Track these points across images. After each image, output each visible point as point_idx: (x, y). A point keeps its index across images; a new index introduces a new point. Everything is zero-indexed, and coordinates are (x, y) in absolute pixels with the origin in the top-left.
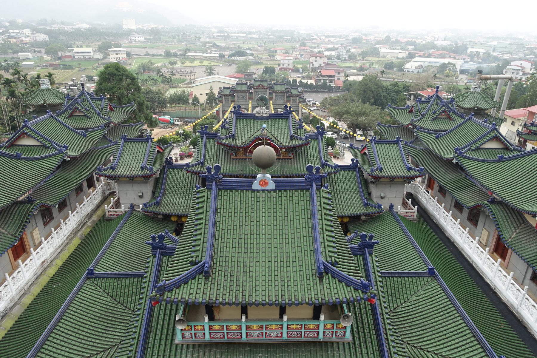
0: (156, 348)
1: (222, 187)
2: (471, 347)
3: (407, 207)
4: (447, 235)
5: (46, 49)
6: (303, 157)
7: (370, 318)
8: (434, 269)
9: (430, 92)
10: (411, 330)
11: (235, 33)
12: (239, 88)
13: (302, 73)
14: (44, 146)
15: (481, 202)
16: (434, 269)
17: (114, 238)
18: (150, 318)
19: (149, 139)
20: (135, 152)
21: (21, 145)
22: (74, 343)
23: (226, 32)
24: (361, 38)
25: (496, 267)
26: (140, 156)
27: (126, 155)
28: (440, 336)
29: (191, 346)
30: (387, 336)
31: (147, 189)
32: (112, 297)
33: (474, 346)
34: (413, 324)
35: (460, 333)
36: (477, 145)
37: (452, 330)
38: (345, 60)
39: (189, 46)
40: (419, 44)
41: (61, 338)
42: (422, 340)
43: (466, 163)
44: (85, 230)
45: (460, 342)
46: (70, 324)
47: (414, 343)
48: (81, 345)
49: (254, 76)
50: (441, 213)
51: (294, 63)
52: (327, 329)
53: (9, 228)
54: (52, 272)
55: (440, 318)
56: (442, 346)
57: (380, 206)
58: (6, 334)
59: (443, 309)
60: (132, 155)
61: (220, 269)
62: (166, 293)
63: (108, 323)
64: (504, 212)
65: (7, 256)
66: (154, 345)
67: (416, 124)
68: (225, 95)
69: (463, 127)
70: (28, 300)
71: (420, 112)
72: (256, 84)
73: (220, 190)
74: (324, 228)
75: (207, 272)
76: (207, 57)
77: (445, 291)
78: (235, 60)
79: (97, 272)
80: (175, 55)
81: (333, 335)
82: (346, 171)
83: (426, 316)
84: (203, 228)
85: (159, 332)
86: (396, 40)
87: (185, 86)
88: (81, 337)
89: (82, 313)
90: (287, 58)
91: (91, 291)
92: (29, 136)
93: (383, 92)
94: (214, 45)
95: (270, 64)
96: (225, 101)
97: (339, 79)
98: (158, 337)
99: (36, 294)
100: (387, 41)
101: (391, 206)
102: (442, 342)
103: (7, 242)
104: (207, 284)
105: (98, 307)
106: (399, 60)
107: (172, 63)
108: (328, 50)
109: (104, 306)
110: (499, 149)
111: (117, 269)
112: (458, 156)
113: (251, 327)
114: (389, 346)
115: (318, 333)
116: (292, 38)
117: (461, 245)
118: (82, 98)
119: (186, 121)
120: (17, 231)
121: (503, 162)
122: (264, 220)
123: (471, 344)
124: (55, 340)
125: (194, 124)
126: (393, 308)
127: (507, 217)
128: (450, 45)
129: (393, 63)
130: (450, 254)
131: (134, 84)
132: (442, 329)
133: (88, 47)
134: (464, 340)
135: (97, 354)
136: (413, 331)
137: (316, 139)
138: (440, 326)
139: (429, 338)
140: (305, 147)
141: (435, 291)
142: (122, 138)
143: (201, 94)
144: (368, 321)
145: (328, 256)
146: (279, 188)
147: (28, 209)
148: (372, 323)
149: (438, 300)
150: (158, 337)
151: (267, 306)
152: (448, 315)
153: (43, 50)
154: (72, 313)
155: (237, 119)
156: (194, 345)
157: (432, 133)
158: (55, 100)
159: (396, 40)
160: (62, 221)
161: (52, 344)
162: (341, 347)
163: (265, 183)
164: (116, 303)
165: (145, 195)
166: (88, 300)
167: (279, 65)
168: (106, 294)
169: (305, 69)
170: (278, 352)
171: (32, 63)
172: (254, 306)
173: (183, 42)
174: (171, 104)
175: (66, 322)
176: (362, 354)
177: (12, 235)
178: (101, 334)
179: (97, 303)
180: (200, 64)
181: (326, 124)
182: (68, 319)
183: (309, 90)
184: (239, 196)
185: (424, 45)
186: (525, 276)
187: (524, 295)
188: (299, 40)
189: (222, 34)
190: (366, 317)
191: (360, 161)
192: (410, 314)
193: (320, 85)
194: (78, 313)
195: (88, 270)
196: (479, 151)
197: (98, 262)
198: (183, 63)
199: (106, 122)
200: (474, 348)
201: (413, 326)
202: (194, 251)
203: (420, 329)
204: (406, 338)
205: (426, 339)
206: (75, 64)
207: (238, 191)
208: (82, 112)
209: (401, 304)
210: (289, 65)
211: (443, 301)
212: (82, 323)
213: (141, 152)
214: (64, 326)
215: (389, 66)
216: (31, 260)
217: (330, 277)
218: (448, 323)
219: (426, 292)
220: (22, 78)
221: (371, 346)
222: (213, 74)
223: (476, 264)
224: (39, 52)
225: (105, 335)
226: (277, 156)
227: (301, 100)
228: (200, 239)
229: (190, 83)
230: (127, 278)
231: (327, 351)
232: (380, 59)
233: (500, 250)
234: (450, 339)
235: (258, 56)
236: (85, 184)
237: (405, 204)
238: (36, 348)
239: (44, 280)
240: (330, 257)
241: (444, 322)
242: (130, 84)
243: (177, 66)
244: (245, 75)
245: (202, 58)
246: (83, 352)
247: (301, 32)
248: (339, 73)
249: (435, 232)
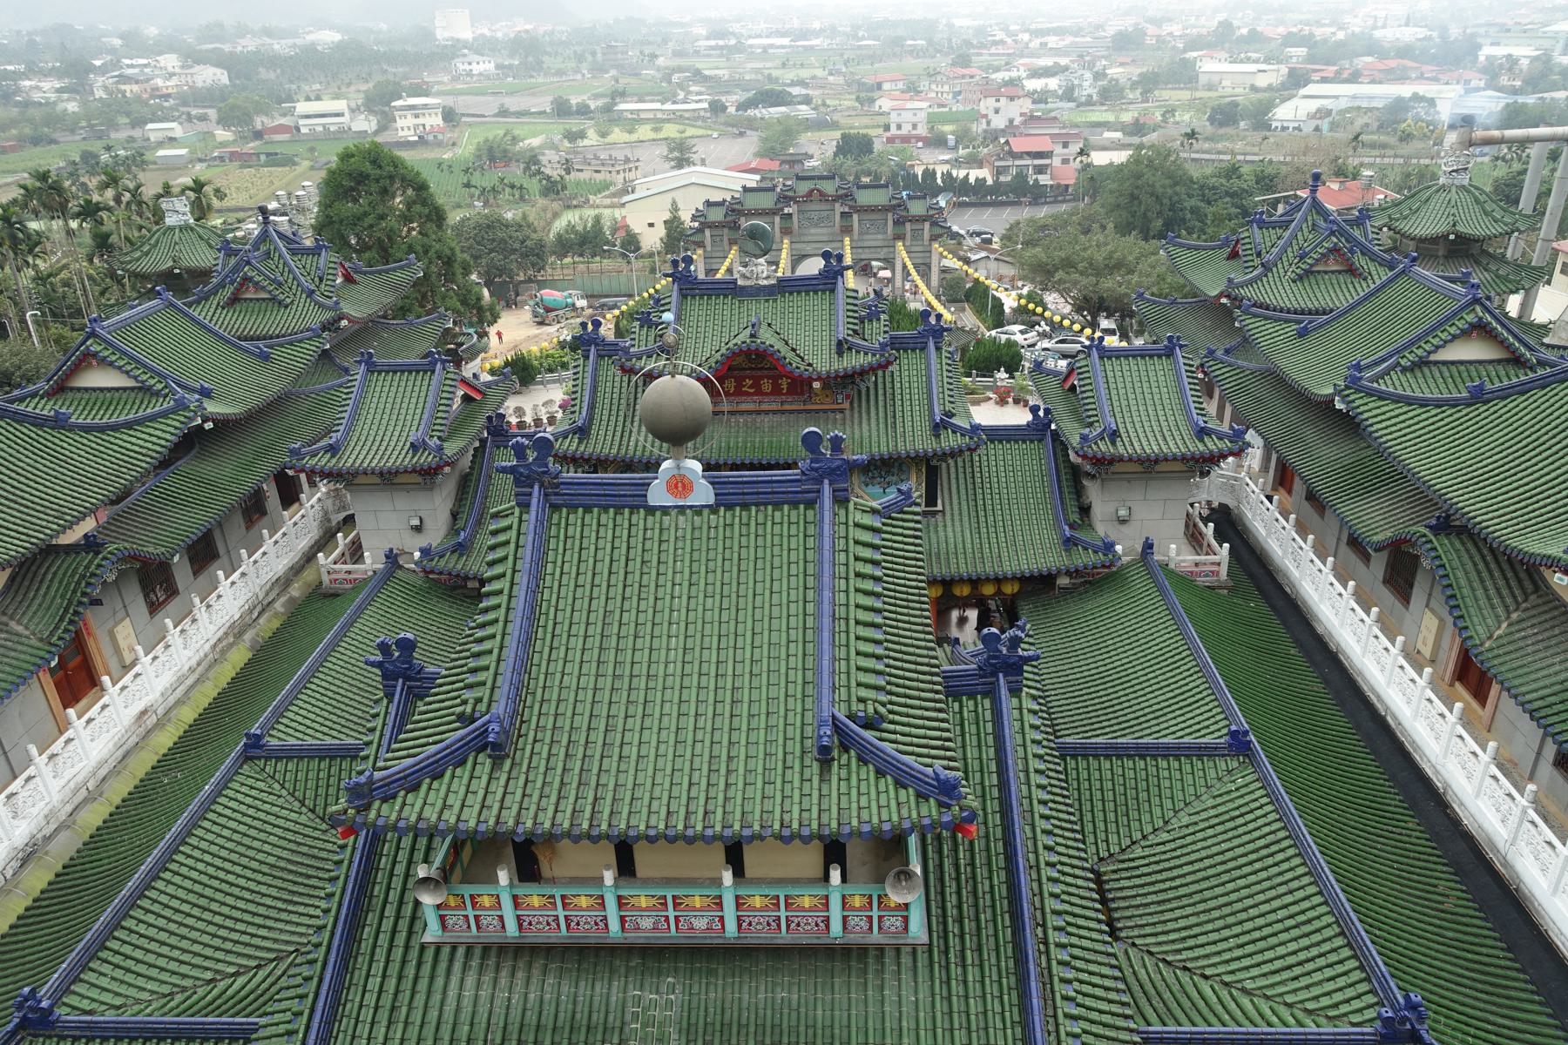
0: (380, 954)
1: (560, 500)
2: (1330, 966)
3: (1201, 546)
4: (1320, 630)
5: (219, 110)
6: (881, 403)
7: (1000, 877)
8: (1246, 733)
9: (253, 227)
10: (1162, 912)
11: (760, 36)
12: (752, 202)
13: (955, 148)
14: (144, 389)
15: (1414, 528)
17: (333, 646)
19: (436, 361)
21: (86, 389)
22: (195, 935)
23: (733, 34)
28: (1244, 933)
29: (478, 951)
30: (1045, 932)
31: (436, 508)
32: (313, 811)
33: (1341, 962)
34: (1171, 894)
35: (1304, 923)
36: (1420, 352)
37: (1281, 914)
38: (1089, 102)
40: (1325, 41)
41: (161, 922)
42: (1191, 942)
43: (1370, 411)
44: (268, 625)
45: (1301, 950)
46: (188, 884)
47: (1166, 952)
48: (217, 942)
49: (809, 164)
51: (932, 120)
52: (853, 909)
53: (36, 620)
54: (165, 740)
55: (1253, 878)
56: (1246, 962)
57: (1109, 547)
58: (27, 909)
59: (1264, 852)
62: (377, 804)
63: (295, 883)
64: (1477, 558)
65: (39, 695)
66: (374, 946)
68: (712, 226)
69: (1383, 296)
70: (94, 817)
71: (1259, 254)
72: (804, 188)
73: (555, 508)
74: (852, 616)
75: (496, 746)
76: (674, 112)
77: (1273, 798)
78: (755, 119)
79: (274, 742)
80: (583, 111)
81: (871, 928)
82: (1016, 441)
83: (1211, 872)
84: (502, 619)
85: (390, 911)
86: (1253, 32)
87: (608, 201)
88: (218, 919)
89: (224, 853)
90: (909, 105)
91: (253, 792)
92: (105, 363)
94: (698, 76)
95: (858, 125)
96: (713, 241)
97: (1065, 161)
98: (387, 925)
99: (117, 800)
100: (1223, 39)
101: (1148, 546)
102: (1250, 949)
103: (28, 658)
105: (272, 839)
106: (1259, 96)
107: (573, 136)
108: (1036, 73)
109: (289, 836)
110: (1491, 362)
111: (334, 733)
112: (1347, 387)
113: (632, 901)
114: (1049, 960)
115: (827, 920)
116: (930, 42)
118: (263, 248)
119: (603, 306)
120: (57, 628)
121: (1485, 403)
123: (1333, 958)
124: (142, 929)
126: (1117, 849)
127: (1485, 574)
128: (1425, 38)
129: (1235, 105)
130: (1319, 687)
131: (424, 203)
132: (1253, 912)
133: (337, 97)
134: (1313, 945)
135: (259, 967)
136: (1168, 916)
137: (922, 349)
138: (1249, 902)
139: (1214, 936)
140: (880, 373)
141: (1247, 798)
142: (359, 362)
143: (651, 225)
144: (992, 886)
145: (854, 699)
146: (725, 500)
147: (87, 567)
148: (1004, 893)
149: (1251, 826)
150: (387, 925)
151: (797, 842)
152: (1276, 870)
153: (212, 113)
154: (196, 853)
155: (683, 295)
156: (486, 949)
157: (1287, 321)
158: (202, 257)
159: (1253, 32)
160: (197, 600)
161: (134, 939)
162: (906, 960)
163: (684, 487)
164: (324, 827)
165: (428, 523)
166: (245, 819)
167: (887, 128)
168: (296, 804)
169: (963, 138)
170: (721, 971)
171: (184, 151)
173: (607, 72)
174: (562, 256)
175: (177, 880)
176: (965, 982)
177: (41, 640)
178: (273, 913)
179: (269, 828)
180: (653, 135)
181: (1009, 302)
182: (184, 870)
183: (973, 199)
184: (611, 525)
185: (1341, 44)
186: (1539, 754)
187: (1524, 812)
189: (721, 43)
190: (986, 875)
191: (1060, 410)
192: (1167, 865)
193: (1007, 184)
194: (214, 855)
196: (1426, 370)
197: (279, 714)
198: (603, 135)
199: (328, 315)
200: (1340, 969)
201: (1169, 900)
202: (470, 687)
203: (1189, 910)
204: (1144, 936)
205: (1202, 940)
206: (301, 149)
207: (607, 512)
208: (263, 288)
209: (1144, 837)
210: (915, 126)
211: (1267, 829)
212: (223, 881)
213: (414, 400)
214: (171, 889)
215: (1225, 115)
216: (104, 707)
217: (854, 761)
218: (1273, 893)
219: (1219, 800)
220: (127, 196)
221: (993, 961)
222: (689, 163)
223: (1395, 718)
224: (203, 118)
225: (284, 916)
226: (715, 403)
227: (938, 231)
229: (625, 192)
231: (880, 972)
232: (1199, 94)
233: (1470, 676)
234: (1273, 941)
235: (824, 104)
237: (1194, 538)
238: (87, 949)
239: (144, 763)
240: (861, 700)
241: (1263, 892)
242: (414, 202)
243: (586, 142)
244: (783, 162)
245: (659, 115)
246: (219, 961)
247: (958, 22)
248: (1065, 145)
249: (1285, 623)
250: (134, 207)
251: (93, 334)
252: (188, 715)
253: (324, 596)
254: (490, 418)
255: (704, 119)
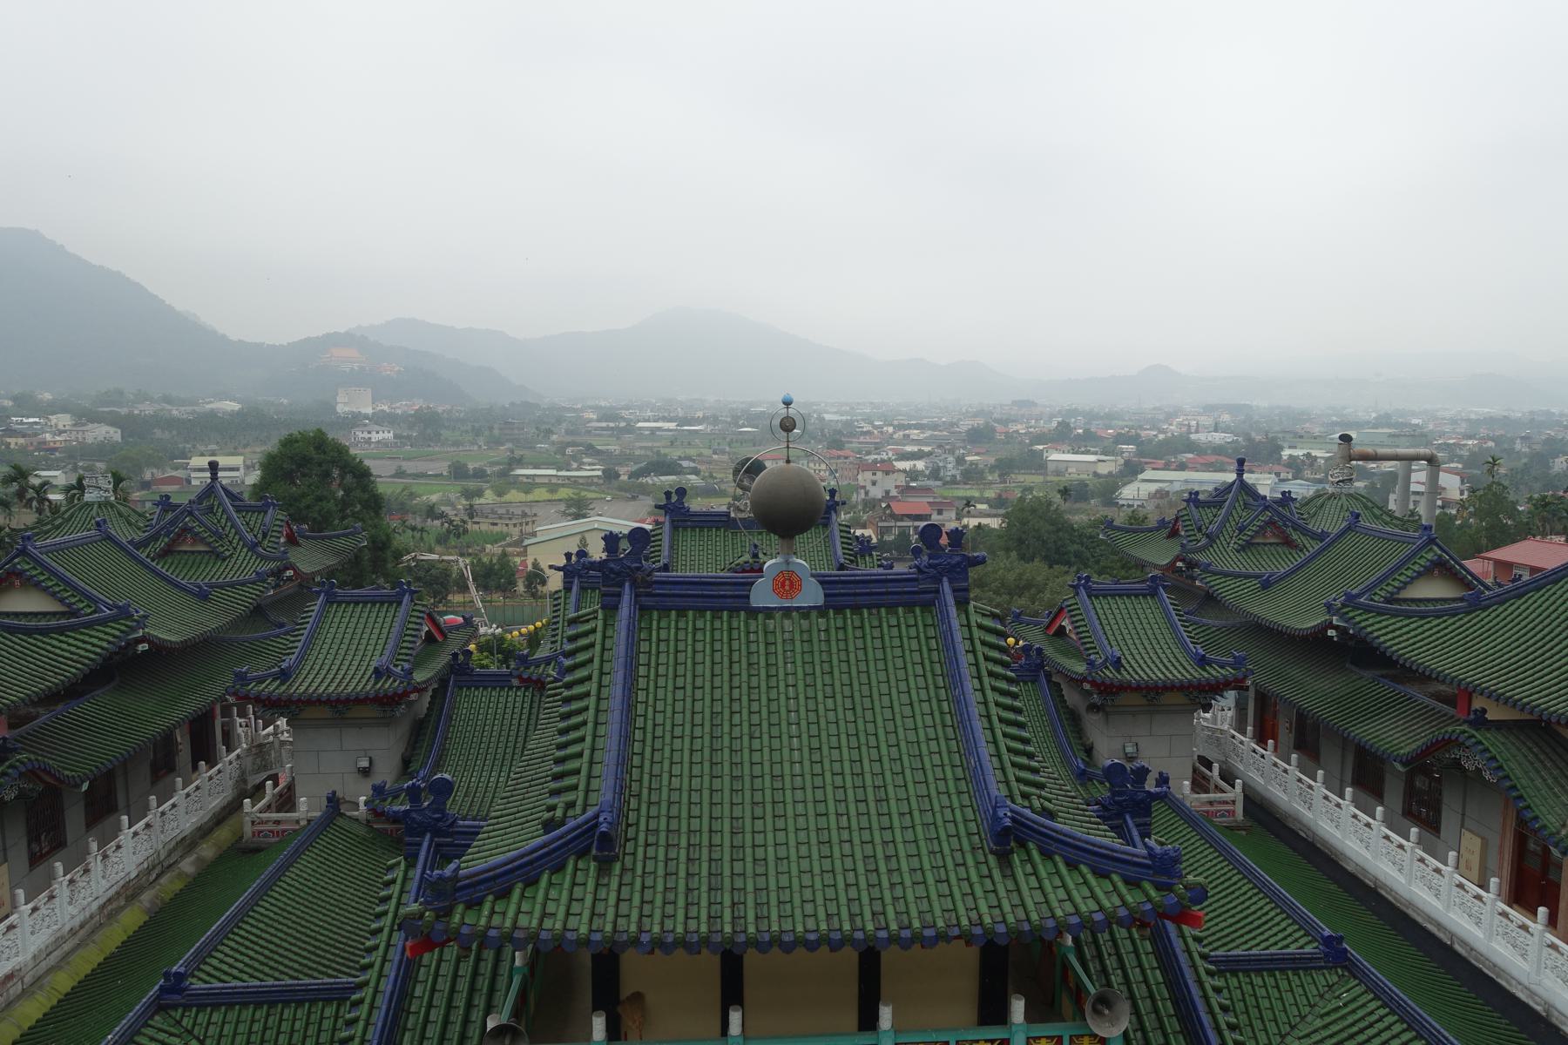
16: (1340, 939)
18: (396, 1018)
19: (404, 592)
20: (359, 631)
24: (993, 430)
25: (1536, 939)
26: (373, 642)
27: (328, 641)
31: (383, 750)
36: (1390, 589)
38: (954, 481)
39: (518, 453)
40: (1150, 441)
44: (169, 885)
50: (1318, 801)
60: (346, 641)
61: (651, 839)
62: (460, 908)
67: (1197, 557)
71: (1200, 529)
76: (569, 478)
80: (480, 474)
86: (1087, 432)
92: (31, 584)
93: (1073, 542)
94: (591, 450)
100: (1063, 435)
104: (607, 885)
107: (468, 494)
117: (1401, 891)
122: (791, 694)
125: (531, 627)
155: (675, 527)
159: (1087, 432)
160: (94, 846)
163: (792, 586)
172: (775, 949)
185: (1162, 444)
188: (823, 435)
195: (167, 975)
197: (201, 958)
208: (203, 540)
213: (376, 631)
219: (1328, 1020)
220: (31, 493)
223: (1464, 943)
228: (580, 755)
230: (300, 1003)
235: (711, 476)
236: (182, 739)
243: (482, 501)
245: (554, 481)
247: (827, 417)
250: (35, 504)
251: (23, 552)
252: (64, 982)
253: (245, 851)
254: (455, 655)
255: (597, 484)
